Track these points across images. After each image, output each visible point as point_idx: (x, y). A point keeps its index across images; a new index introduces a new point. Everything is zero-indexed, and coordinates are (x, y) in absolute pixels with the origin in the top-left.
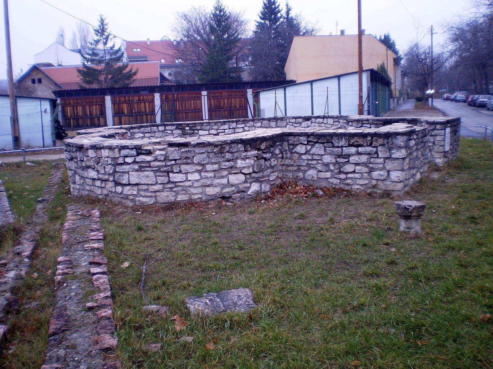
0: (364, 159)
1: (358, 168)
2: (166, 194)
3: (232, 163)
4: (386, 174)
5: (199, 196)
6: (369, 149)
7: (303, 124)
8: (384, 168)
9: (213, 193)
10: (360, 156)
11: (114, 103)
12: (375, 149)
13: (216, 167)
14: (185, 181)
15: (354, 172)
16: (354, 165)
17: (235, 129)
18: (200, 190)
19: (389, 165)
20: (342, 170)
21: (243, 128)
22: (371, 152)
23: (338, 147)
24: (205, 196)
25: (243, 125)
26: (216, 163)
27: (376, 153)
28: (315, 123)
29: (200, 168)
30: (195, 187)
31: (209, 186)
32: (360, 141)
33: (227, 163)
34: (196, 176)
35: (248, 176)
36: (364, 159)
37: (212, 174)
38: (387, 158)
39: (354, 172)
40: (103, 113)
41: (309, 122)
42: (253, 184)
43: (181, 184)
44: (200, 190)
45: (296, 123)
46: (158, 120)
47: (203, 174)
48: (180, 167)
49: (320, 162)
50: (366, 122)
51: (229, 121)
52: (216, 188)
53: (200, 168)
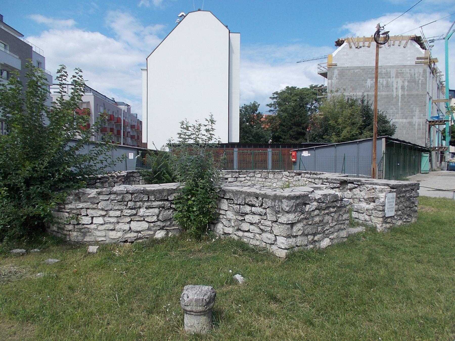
0: (256, 219)
1: (252, 227)
2: (75, 234)
3: (134, 212)
4: (273, 238)
5: (103, 239)
6: (259, 210)
7: (295, 177)
8: (271, 232)
9: (115, 237)
10: (253, 216)
11: (239, 154)
12: (264, 211)
13: (118, 213)
14: (91, 224)
15: (248, 231)
16: (249, 224)
17: (237, 178)
18: (103, 233)
19: (277, 229)
20: (240, 228)
21: (245, 177)
22: (261, 213)
23: (237, 204)
24: (109, 239)
25: (245, 175)
26: (119, 210)
27: (265, 214)
28: (304, 177)
29: (104, 213)
30: (99, 230)
31: (111, 230)
32: (253, 201)
33: (129, 211)
34: (100, 220)
35: (152, 224)
36: (256, 219)
37: (114, 220)
38: (274, 221)
39: (248, 231)
40: (265, 161)
41: (300, 177)
42: (158, 232)
43: (87, 226)
44: (103, 233)
45: (290, 177)
46: (235, 167)
47: (107, 219)
48: (87, 211)
49: (225, 217)
50: (326, 181)
51: (232, 172)
52: (119, 233)
53: (104, 213)
